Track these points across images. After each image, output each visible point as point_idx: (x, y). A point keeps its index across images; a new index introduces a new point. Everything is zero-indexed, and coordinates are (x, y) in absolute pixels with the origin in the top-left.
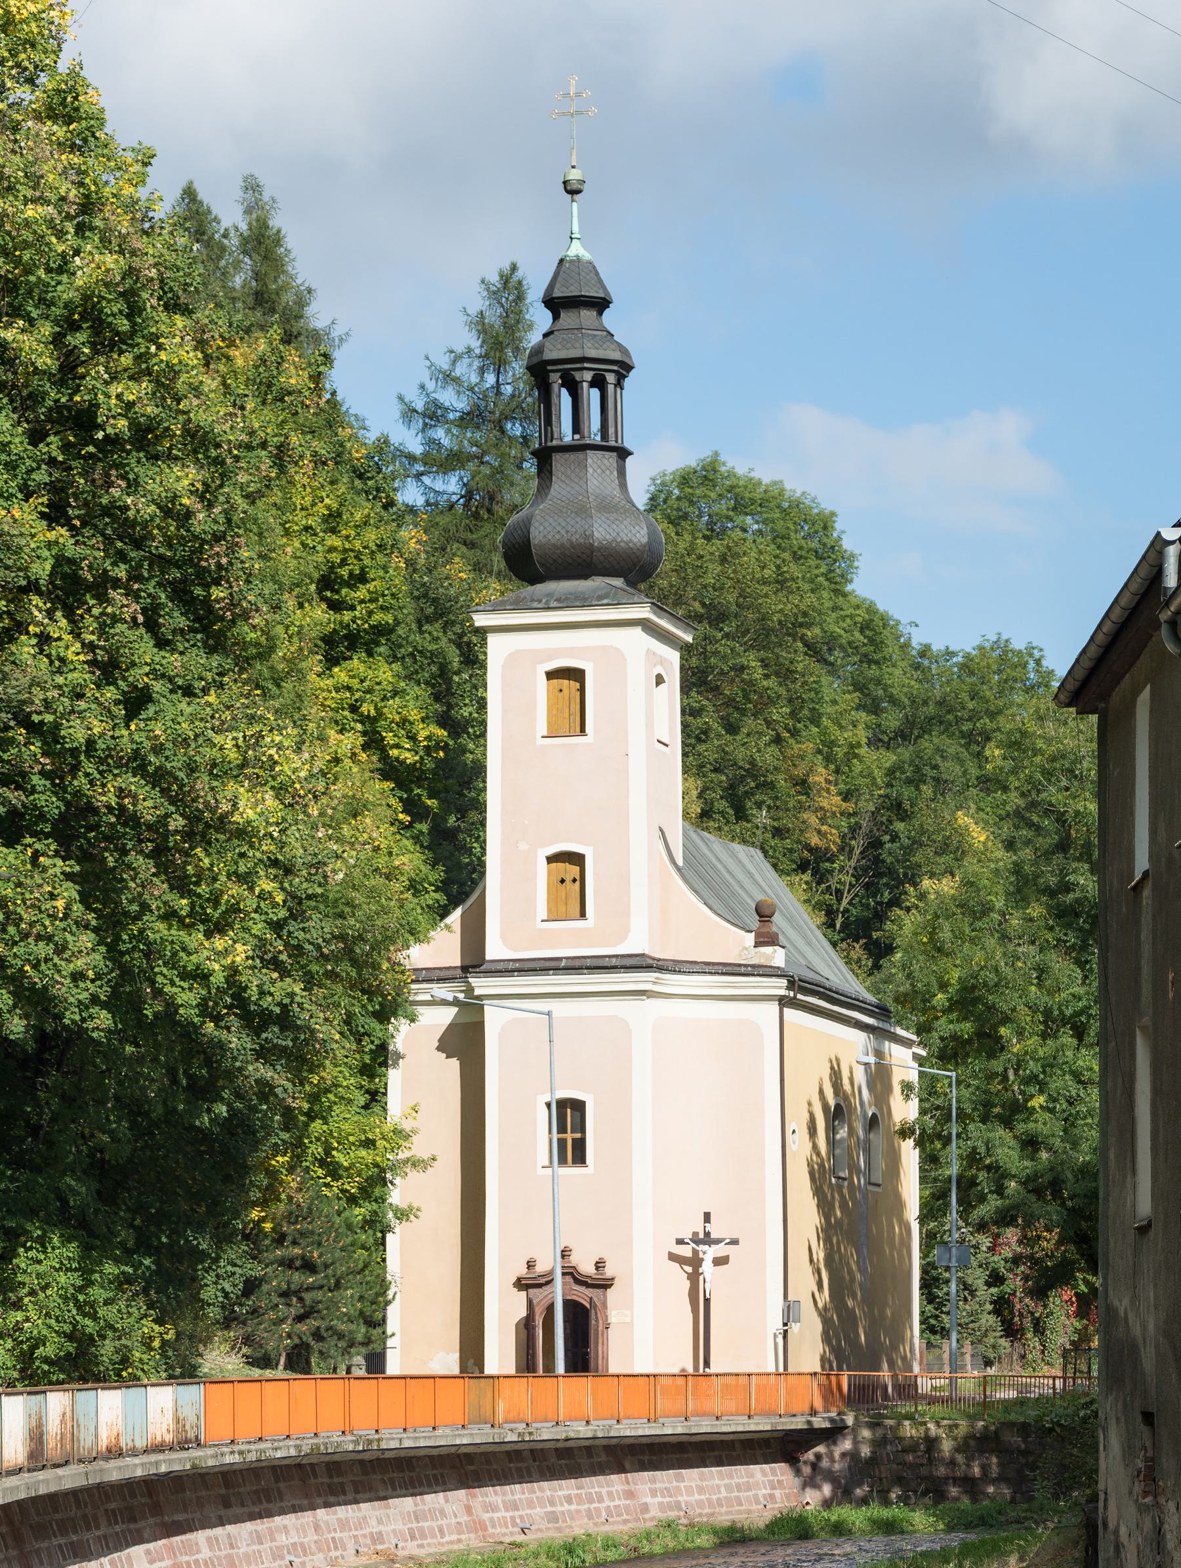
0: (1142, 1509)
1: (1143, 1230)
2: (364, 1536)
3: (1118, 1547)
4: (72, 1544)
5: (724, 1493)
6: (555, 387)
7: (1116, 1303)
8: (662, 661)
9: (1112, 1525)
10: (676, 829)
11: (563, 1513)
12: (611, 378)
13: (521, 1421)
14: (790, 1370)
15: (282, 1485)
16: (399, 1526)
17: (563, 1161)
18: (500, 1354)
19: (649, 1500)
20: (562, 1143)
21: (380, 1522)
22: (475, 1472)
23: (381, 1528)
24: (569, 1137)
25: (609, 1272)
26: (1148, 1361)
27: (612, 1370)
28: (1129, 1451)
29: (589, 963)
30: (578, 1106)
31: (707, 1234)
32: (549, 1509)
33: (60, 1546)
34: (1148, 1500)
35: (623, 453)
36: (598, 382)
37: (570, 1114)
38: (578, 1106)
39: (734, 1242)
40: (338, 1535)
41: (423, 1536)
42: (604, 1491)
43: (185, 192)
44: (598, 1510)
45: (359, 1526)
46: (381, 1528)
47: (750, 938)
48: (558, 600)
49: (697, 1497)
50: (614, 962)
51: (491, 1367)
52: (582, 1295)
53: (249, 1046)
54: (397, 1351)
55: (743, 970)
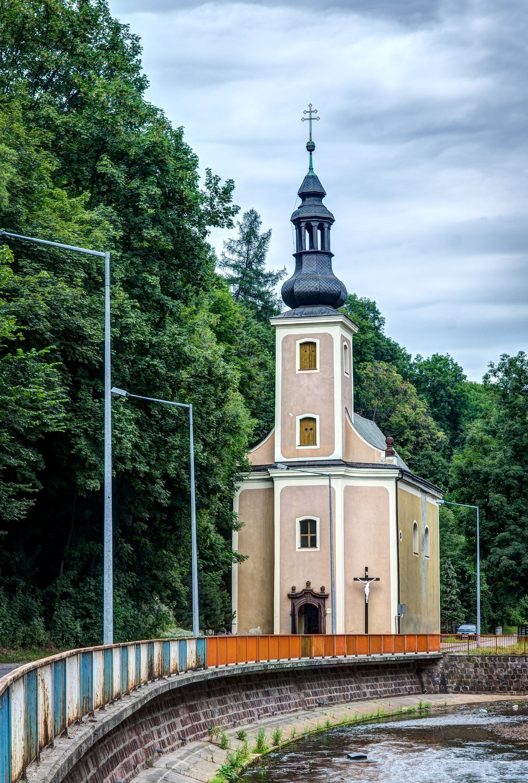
2: (261, 709)
4: (153, 718)
5: (394, 687)
6: (303, 228)
8: (347, 340)
11: (334, 697)
12: (326, 225)
14: (370, 633)
15: (229, 686)
16: (274, 704)
19: (366, 690)
21: (266, 703)
22: (300, 679)
23: (267, 705)
24: (309, 535)
27: (329, 632)
29: (317, 463)
31: (367, 576)
32: (329, 695)
33: (149, 720)
35: (331, 255)
37: (308, 527)
39: (378, 579)
40: (251, 709)
41: (283, 709)
42: (349, 686)
44: (347, 695)
45: (259, 705)
46: (267, 705)
47: (383, 454)
48: (305, 314)
49: (384, 689)
50: (328, 463)
51: (277, 631)
54: (237, 625)
55: (381, 466)
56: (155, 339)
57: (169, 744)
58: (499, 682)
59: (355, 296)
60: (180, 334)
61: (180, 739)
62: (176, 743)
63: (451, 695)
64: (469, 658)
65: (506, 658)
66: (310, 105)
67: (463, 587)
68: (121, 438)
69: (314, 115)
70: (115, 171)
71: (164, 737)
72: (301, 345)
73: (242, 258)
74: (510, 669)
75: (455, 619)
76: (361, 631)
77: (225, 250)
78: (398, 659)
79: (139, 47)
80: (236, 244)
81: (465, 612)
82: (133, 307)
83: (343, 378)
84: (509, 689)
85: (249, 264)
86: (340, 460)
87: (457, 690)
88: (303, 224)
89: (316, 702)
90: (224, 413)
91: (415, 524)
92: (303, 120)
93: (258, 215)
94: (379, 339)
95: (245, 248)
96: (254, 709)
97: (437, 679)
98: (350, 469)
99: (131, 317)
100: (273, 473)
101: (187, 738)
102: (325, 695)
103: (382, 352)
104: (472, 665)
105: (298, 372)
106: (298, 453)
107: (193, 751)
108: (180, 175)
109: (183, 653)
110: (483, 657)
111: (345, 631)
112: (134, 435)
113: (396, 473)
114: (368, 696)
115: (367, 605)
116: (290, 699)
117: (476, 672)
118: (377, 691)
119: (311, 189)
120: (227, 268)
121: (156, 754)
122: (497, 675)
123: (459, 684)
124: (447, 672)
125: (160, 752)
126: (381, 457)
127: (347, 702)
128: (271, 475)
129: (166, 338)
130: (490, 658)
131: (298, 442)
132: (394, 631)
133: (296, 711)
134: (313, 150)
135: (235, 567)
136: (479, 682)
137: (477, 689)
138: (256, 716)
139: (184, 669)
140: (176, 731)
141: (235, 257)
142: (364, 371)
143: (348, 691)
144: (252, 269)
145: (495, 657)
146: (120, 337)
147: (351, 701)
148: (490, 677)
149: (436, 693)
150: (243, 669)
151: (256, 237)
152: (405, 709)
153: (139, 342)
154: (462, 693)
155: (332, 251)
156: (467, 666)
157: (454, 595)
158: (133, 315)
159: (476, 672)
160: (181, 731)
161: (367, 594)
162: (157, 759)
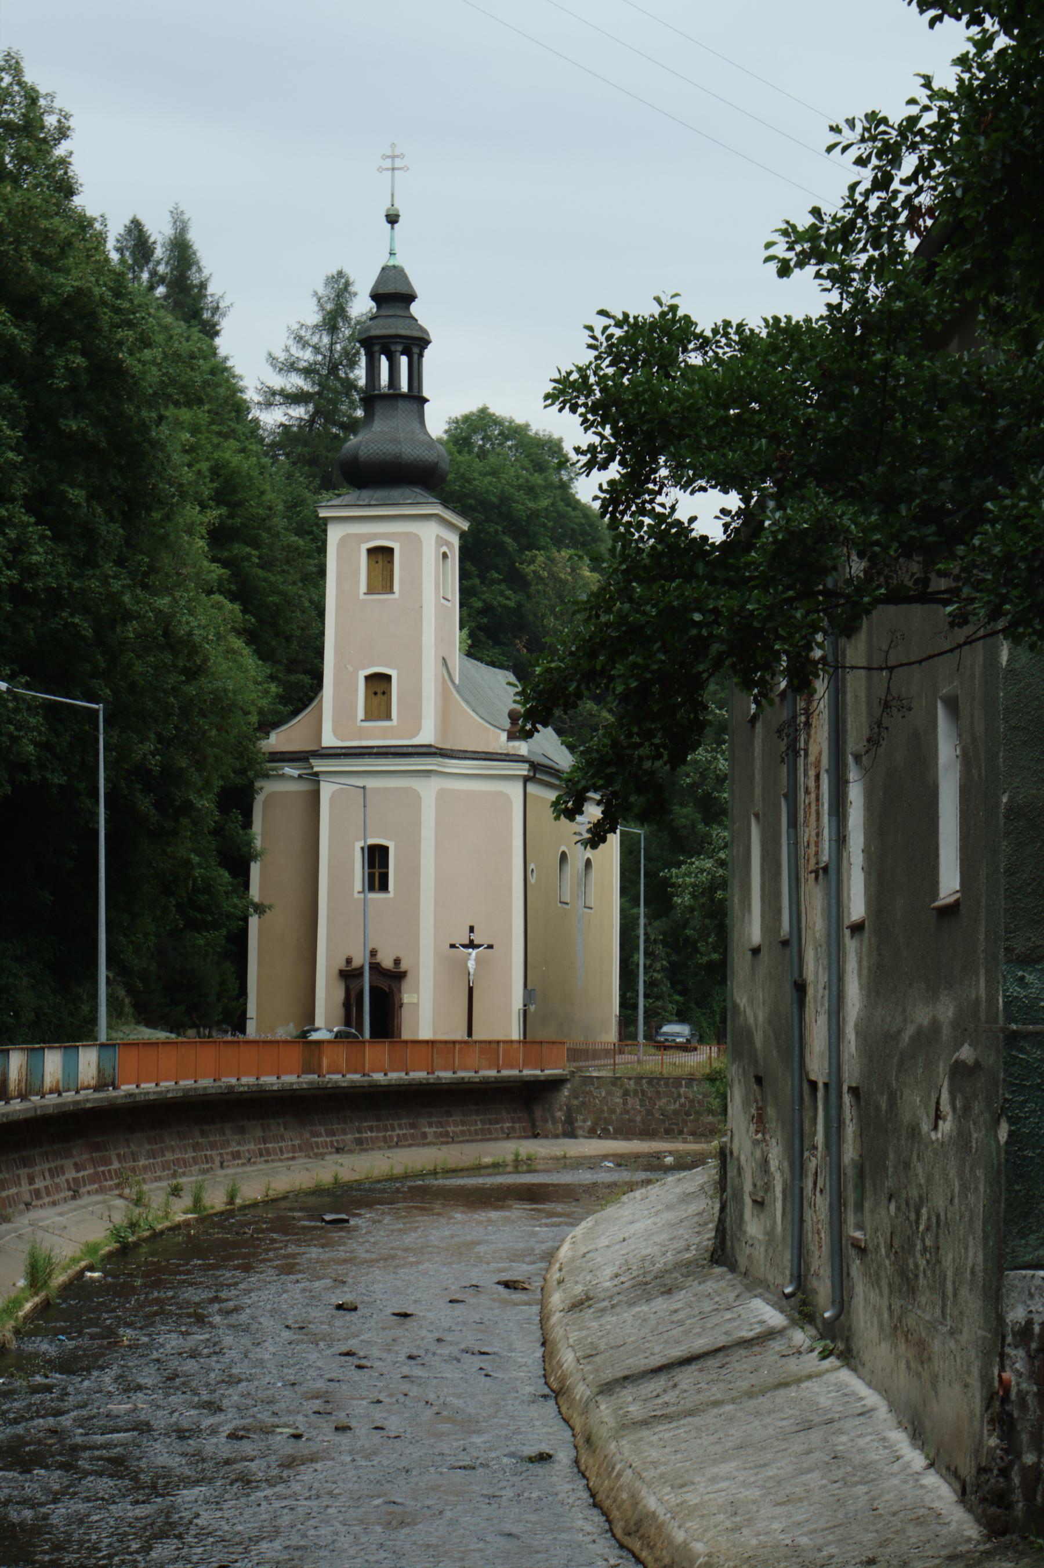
0: (756, 1143)
1: (756, 951)
3: (740, 1169)
7: (738, 1001)
8: (447, 543)
9: (735, 1154)
10: (456, 658)
12: (416, 350)
13: (338, 1073)
17: (372, 889)
18: (326, 1023)
19: (427, 1130)
20: (371, 876)
25: (403, 967)
26: (759, 1043)
27: (406, 1035)
28: (746, 1103)
29: (392, 750)
30: (384, 850)
31: (472, 941)
34: (760, 1136)
36: (407, 352)
37: (377, 858)
38: (384, 850)
39: (490, 947)
41: (268, 1154)
43: (129, 231)
47: (504, 736)
50: (410, 750)
52: (384, 984)
53: (201, 362)
56: (76, 584)
57: (48, 1194)
58: (663, 1121)
59: (527, 425)
60: (115, 577)
61: (69, 1189)
62: (62, 1195)
63: (582, 1140)
64: (615, 1081)
65: (677, 1081)
66: (393, 145)
67: (674, 958)
68: (19, 738)
69: (398, 163)
70: (16, 331)
71: (39, 1184)
72: (371, 551)
73: (320, 358)
74: (683, 1100)
75: (658, 1014)
76: (461, 1035)
77: (290, 342)
78: (485, 1082)
79: (69, 128)
80: (309, 333)
81: (677, 1002)
82: (43, 537)
83: (439, 607)
84: (681, 1132)
85: (333, 369)
86: (430, 746)
87: (592, 1133)
88: (377, 348)
89: (332, 1146)
90: (201, 688)
91: (564, 855)
92: (381, 170)
93: (351, 280)
94: (568, 505)
95: (326, 340)
96: (214, 1153)
97: (559, 1114)
98: (447, 761)
99: (38, 554)
100: (319, 766)
101: (83, 1190)
102: (349, 1136)
103: (573, 530)
104: (619, 1093)
105: (362, 597)
106: (361, 734)
107: (85, 1207)
108: (118, 337)
109: (167, 1067)
110: (639, 1079)
111: (435, 1034)
112: (40, 732)
113: (523, 770)
114: (430, 1139)
115: (471, 989)
116: (283, 1139)
117: (625, 1103)
118: (447, 1133)
119: (390, 289)
120: (293, 374)
121: (22, 1206)
122: (660, 1109)
123: (595, 1124)
124: (576, 1102)
125: (28, 1205)
126: (500, 741)
127: (390, 1147)
128: (316, 769)
129: (94, 584)
130: (650, 1081)
131: (361, 714)
132: (516, 1034)
133: (293, 1158)
134: (396, 222)
135: (254, 922)
136: (631, 1120)
137: (625, 1132)
138: (217, 1163)
139: (72, 1086)
140: (64, 1178)
141: (307, 356)
142: (532, 567)
143: (393, 1130)
144: (338, 378)
145: (659, 1079)
146: (21, 582)
147: (397, 1145)
148: (649, 1112)
149: (557, 1137)
150: (186, 1091)
151: (346, 318)
152: (487, 1160)
153: (49, 590)
154: (600, 1137)
155: (426, 393)
156: (610, 1093)
157: (658, 972)
158: (41, 550)
159: (625, 1103)
160: (74, 1179)
161: (472, 971)
162: (21, 1213)
